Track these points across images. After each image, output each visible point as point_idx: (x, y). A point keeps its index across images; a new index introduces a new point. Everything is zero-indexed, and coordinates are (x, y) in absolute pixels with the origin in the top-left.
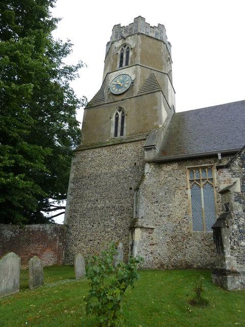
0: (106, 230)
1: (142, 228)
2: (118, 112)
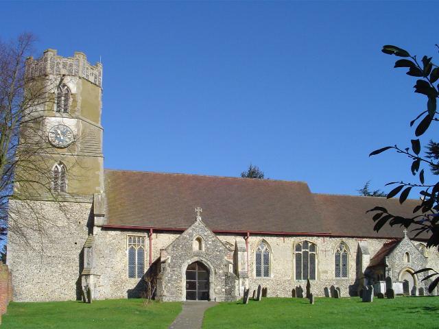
0: (54, 274)
1: (94, 275)
2: (58, 166)
